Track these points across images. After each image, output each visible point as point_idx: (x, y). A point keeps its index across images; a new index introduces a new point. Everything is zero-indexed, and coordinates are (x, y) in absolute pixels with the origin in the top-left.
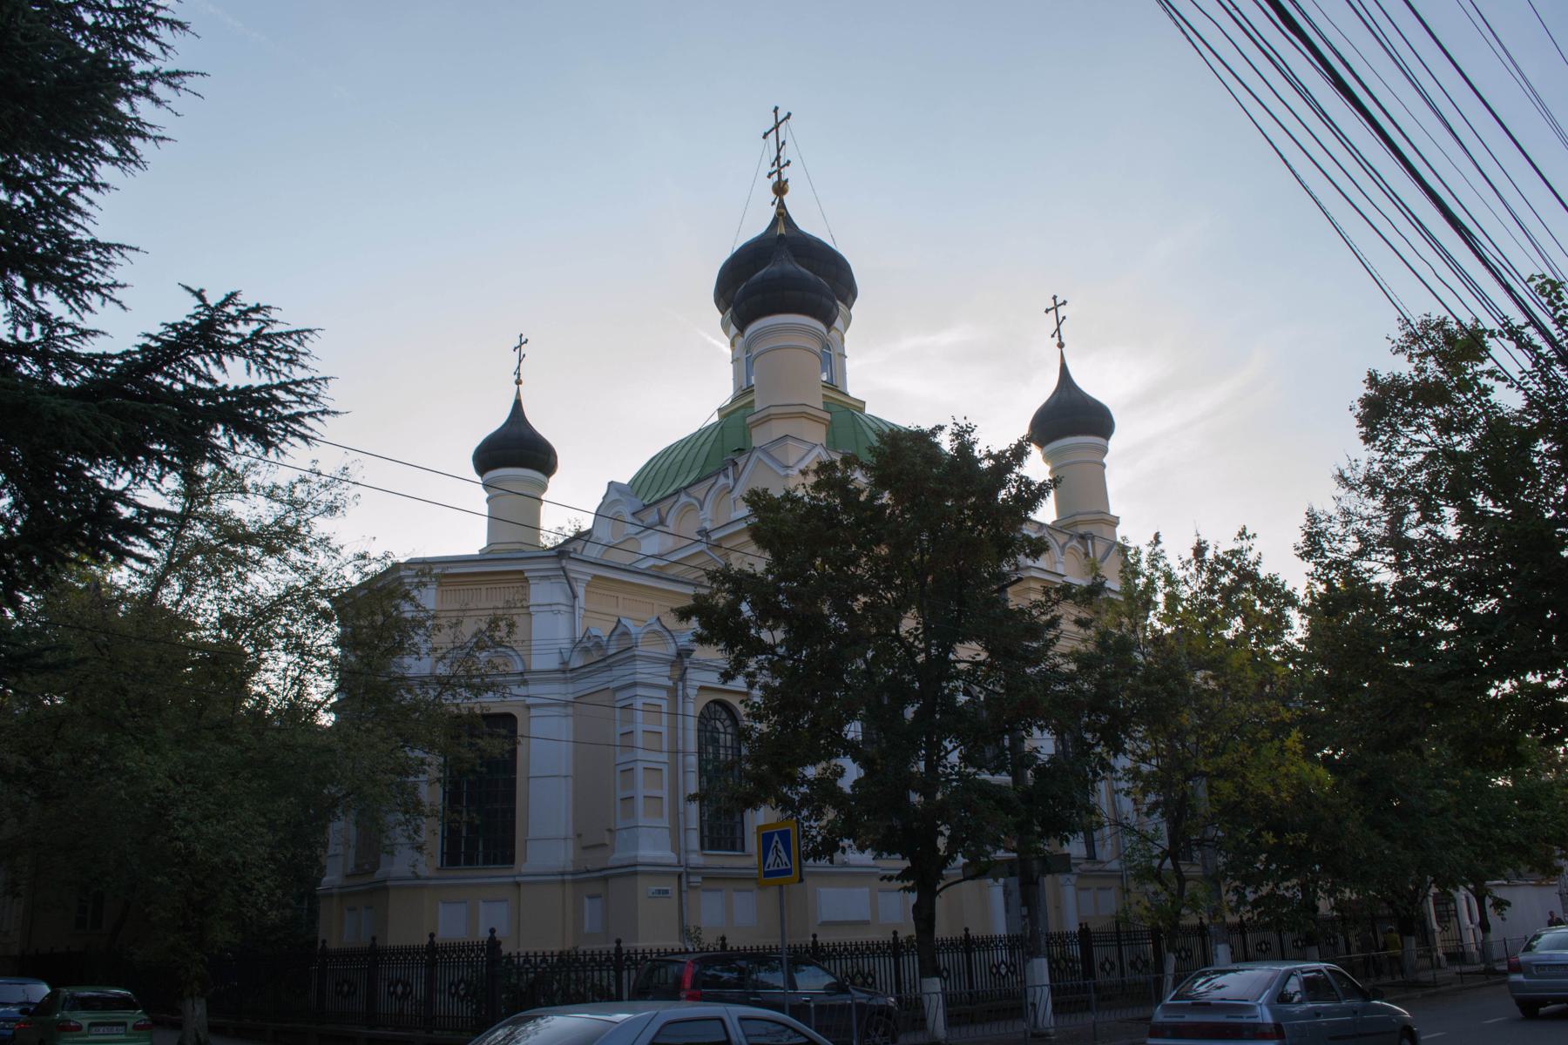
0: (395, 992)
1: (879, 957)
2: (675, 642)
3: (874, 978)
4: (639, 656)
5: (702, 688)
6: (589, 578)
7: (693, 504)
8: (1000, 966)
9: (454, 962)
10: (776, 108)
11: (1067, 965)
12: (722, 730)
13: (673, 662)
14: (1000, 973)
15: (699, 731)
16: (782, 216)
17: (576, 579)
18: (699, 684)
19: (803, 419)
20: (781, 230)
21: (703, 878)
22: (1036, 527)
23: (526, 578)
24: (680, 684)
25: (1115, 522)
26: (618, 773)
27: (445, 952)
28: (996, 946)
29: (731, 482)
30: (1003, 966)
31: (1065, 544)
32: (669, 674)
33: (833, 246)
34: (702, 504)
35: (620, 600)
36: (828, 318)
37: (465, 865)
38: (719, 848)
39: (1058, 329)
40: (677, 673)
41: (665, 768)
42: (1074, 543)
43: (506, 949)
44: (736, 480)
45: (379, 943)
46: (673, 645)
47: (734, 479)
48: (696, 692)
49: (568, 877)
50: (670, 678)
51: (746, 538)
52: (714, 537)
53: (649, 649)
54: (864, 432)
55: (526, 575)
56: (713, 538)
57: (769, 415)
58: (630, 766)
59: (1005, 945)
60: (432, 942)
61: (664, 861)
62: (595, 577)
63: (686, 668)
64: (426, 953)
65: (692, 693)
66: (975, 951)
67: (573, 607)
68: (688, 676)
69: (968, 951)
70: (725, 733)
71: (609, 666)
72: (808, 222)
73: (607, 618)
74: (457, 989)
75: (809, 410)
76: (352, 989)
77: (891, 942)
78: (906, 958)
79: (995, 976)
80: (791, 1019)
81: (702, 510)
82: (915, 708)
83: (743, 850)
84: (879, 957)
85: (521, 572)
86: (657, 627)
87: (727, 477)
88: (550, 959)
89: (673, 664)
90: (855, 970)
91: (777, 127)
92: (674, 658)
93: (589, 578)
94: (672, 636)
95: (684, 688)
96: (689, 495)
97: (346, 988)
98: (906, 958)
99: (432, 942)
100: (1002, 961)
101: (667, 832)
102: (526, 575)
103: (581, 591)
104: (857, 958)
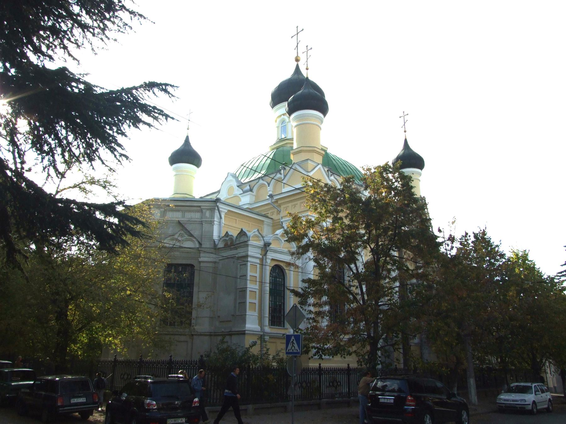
0: (123, 378)
2: (264, 240)
3: (340, 383)
4: (250, 245)
5: (272, 260)
6: (227, 211)
7: (265, 184)
9: (155, 367)
10: (297, 27)
11: (337, 384)
13: (262, 248)
15: (270, 277)
17: (222, 211)
18: (271, 258)
19: (315, 153)
21: (270, 337)
23: (202, 209)
24: (264, 257)
28: (337, 373)
29: (282, 176)
30: (304, 383)
32: (260, 253)
34: (269, 184)
35: (237, 221)
37: (169, 326)
38: (274, 326)
39: (405, 123)
40: (263, 253)
41: (257, 291)
44: (285, 176)
46: (263, 241)
47: (284, 176)
48: (270, 261)
49: (212, 334)
50: (261, 254)
52: (275, 198)
53: (255, 242)
54: (331, 160)
56: (275, 198)
57: (301, 150)
60: (171, 360)
61: (256, 330)
62: (229, 211)
63: (268, 251)
64: (167, 364)
65: (269, 261)
66: (323, 375)
67: (220, 222)
68: (267, 254)
69: (320, 375)
73: (237, 229)
75: (316, 149)
77: (318, 368)
80: (526, 385)
81: (269, 186)
83: (284, 327)
85: (200, 207)
86: (257, 233)
87: (281, 174)
91: (297, 34)
92: (263, 246)
93: (227, 211)
95: (266, 258)
96: (263, 180)
101: (257, 317)
102: (202, 207)
103: (223, 216)
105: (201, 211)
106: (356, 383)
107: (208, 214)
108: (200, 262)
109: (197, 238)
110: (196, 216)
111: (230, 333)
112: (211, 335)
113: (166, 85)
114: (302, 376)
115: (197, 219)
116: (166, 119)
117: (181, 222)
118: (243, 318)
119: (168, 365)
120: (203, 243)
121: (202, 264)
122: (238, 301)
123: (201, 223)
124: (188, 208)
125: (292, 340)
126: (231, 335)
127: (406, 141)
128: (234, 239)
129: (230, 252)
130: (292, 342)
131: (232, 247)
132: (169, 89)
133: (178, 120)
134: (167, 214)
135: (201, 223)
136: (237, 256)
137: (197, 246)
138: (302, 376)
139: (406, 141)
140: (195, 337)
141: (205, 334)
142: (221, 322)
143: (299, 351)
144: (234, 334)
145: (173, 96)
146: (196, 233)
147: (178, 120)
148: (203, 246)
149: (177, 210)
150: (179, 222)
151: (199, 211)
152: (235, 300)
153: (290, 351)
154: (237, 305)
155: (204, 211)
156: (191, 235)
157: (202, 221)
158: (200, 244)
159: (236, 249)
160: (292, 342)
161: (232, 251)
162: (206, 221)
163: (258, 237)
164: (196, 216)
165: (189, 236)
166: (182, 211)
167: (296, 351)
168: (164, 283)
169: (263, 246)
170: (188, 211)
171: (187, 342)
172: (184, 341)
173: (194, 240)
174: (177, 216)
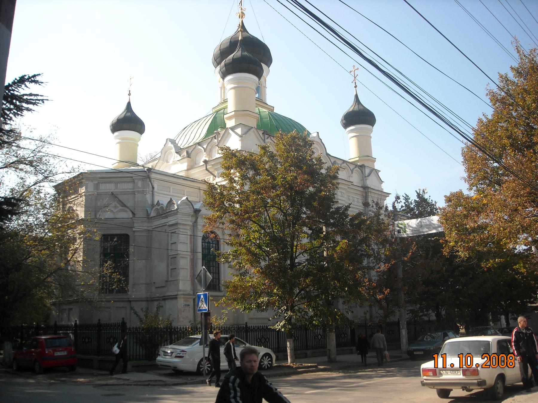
1: (254, 332)
8: (318, 336)
12: (211, 242)
14: (318, 339)
16: (243, 27)
20: (129, 114)
22: (342, 161)
23: (134, 179)
25: (374, 160)
26: (170, 259)
27: (108, 326)
31: (353, 169)
33: (263, 41)
36: (259, 73)
42: (357, 169)
43: (128, 325)
45: (58, 323)
49: (149, 299)
51: (219, 166)
55: (134, 178)
58: (175, 256)
59: (321, 328)
60: (99, 323)
68: (198, 221)
70: (213, 244)
71: (166, 216)
72: (253, 31)
74: (345, 336)
76: (90, 340)
78: (251, 333)
79: (316, 339)
82: (466, 192)
84: (254, 332)
85: (132, 177)
88: (139, 329)
89: (192, 216)
90: (257, 338)
94: (192, 205)
97: (87, 340)
98: (251, 333)
99: (99, 323)
100: (319, 334)
102: (134, 178)
104: (267, 331)
105: (134, 182)
106: (270, 340)
107: (140, 184)
108: (134, 232)
109: (130, 208)
110: (128, 187)
111: (164, 298)
112: (148, 301)
113: (34, 76)
114: (274, 347)
115: (130, 189)
116: (43, 102)
117: (114, 193)
118: (176, 282)
119: (97, 328)
120: (136, 213)
121: (136, 234)
122: (170, 267)
123: (134, 193)
124: (119, 179)
125: (201, 299)
126: (164, 300)
127: (356, 96)
128: (165, 208)
129: (162, 220)
130: (202, 300)
131: (163, 216)
132: (37, 78)
133: (129, 95)
134: (100, 186)
135: (134, 193)
136: (167, 224)
137: (131, 215)
138: (274, 347)
139: (356, 96)
140: (132, 302)
141: (142, 299)
142: (156, 288)
143: (206, 308)
144: (168, 299)
145: (43, 83)
146: (129, 204)
147: (129, 95)
148: (137, 216)
149: (110, 182)
150: (112, 193)
151: (132, 181)
152: (168, 266)
153: (200, 309)
154: (170, 271)
155: (136, 181)
156: (124, 205)
157: (134, 191)
158: (134, 214)
159: (167, 217)
160: (202, 300)
161: (164, 220)
162: (138, 191)
163: (188, 205)
164: (128, 187)
165: (122, 206)
166: (115, 182)
167: (204, 308)
168: (101, 253)
169: (193, 214)
170: (120, 182)
171: (126, 307)
172: (123, 307)
173: (127, 209)
174: (110, 188)
